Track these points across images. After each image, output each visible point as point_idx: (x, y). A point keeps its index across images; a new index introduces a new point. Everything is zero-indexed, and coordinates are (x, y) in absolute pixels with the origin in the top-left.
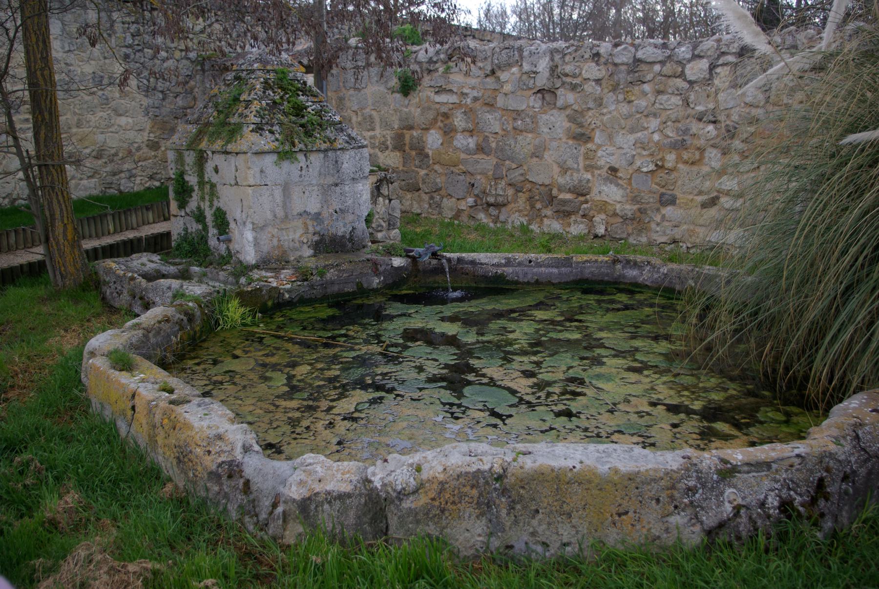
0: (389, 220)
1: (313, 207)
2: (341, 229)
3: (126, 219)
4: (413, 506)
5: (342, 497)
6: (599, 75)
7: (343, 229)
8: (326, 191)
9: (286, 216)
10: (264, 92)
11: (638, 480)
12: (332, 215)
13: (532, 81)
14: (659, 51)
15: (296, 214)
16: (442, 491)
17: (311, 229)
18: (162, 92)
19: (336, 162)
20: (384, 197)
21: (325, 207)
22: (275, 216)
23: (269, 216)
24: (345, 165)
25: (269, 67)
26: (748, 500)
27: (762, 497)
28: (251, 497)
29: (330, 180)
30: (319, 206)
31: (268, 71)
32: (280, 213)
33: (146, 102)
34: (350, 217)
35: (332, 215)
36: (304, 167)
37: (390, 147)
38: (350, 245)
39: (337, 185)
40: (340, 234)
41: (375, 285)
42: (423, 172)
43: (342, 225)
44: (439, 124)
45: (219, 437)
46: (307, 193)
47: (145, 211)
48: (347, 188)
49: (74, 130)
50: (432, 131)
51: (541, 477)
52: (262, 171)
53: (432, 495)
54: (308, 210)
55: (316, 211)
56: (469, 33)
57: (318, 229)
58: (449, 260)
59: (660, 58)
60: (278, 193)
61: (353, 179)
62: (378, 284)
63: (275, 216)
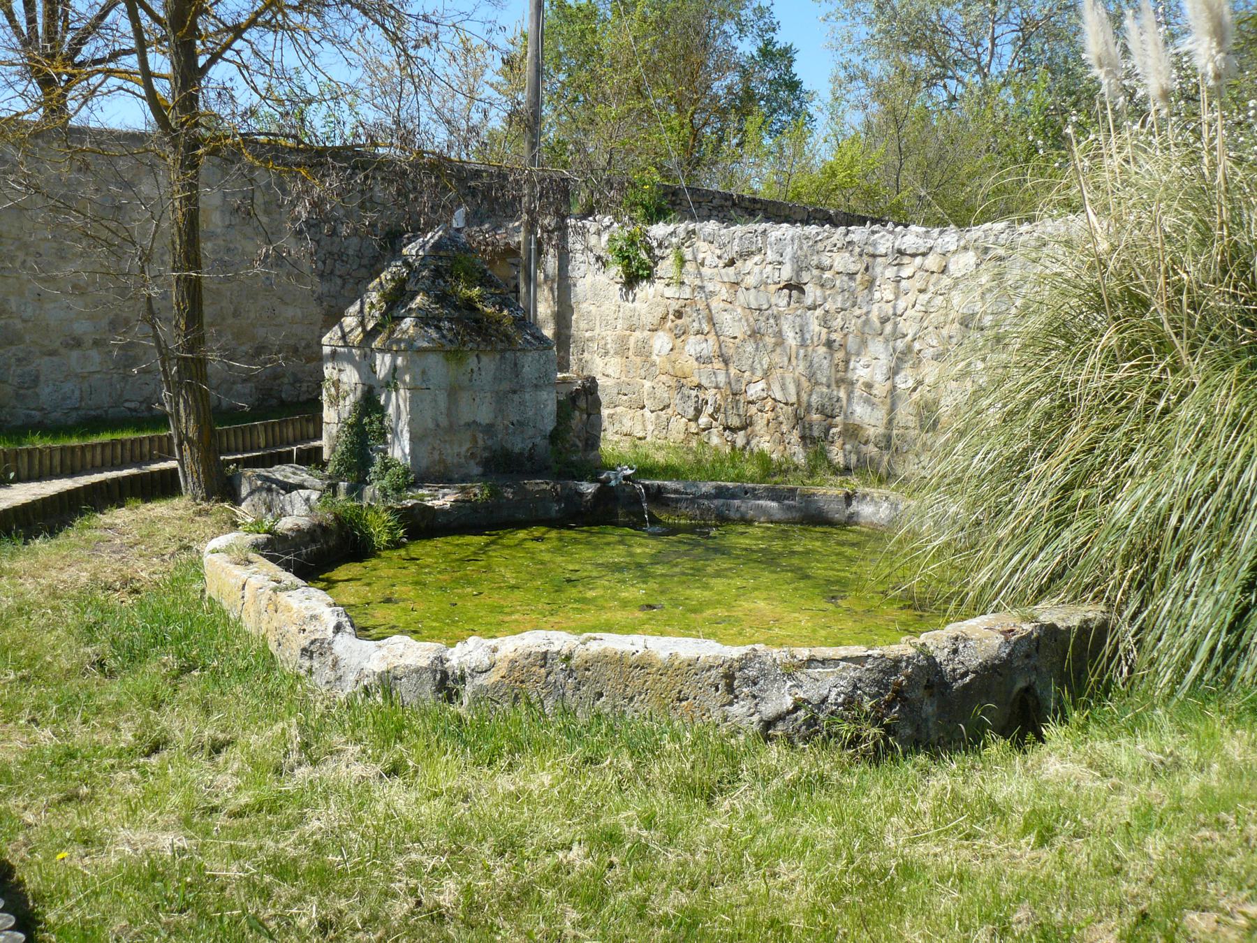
0: (587, 440)
1: (484, 414)
2: (518, 445)
3: (281, 432)
4: (485, 683)
5: (419, 671)
6: (853, 268)
7: (520, 446)
8: (501, 399)
9: (451, 426)
10: (433, 282)
11: (698, 666)
12: (507, 428)
13: (777, 274)
14: (921, 241)
15: (462, 423)
16: (511, 670)
17: (480, 443)
18: (340, 277)
19: (516, 365)
20: (581, 411)
21: (499, 418)
22: (438, 425)
23: (431, 425)
24: (526, 369)
25: (442, 253)
26: (810, 694)
27: (826, 692)
28: (340, 673)
29: (505, 386)
30: (492, 416)
31: (441, 258)
32: (444, 422)
33: (321, 288)
34: (531, 432)
35: (507, 428)
36: (476, 369)
37: (612, 352)
38: (528, 465)
39: (515, 392)
40: (517, 450)
41: (553, 514)
42: (648, 384)
43: (519, 440)
44: (669, 324)
45: (314, 617)
46: (477, 400)
47: (304, 423)
48: (527, 396)
49: (230, 321)
50: (660, 333)
51: (604, 660)
52: (424, 372)
53: (503, 672)
54: (478, 420)
55: (487, 421)
56: (759, 206)
57: (489, 443)
58: (645, 487)
59: (922, 250)
60: (442, 399)
61: (536, 386)
62: (557, 512)
63: (438, 425)
